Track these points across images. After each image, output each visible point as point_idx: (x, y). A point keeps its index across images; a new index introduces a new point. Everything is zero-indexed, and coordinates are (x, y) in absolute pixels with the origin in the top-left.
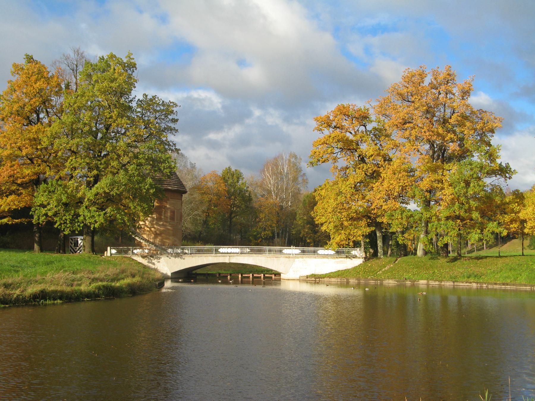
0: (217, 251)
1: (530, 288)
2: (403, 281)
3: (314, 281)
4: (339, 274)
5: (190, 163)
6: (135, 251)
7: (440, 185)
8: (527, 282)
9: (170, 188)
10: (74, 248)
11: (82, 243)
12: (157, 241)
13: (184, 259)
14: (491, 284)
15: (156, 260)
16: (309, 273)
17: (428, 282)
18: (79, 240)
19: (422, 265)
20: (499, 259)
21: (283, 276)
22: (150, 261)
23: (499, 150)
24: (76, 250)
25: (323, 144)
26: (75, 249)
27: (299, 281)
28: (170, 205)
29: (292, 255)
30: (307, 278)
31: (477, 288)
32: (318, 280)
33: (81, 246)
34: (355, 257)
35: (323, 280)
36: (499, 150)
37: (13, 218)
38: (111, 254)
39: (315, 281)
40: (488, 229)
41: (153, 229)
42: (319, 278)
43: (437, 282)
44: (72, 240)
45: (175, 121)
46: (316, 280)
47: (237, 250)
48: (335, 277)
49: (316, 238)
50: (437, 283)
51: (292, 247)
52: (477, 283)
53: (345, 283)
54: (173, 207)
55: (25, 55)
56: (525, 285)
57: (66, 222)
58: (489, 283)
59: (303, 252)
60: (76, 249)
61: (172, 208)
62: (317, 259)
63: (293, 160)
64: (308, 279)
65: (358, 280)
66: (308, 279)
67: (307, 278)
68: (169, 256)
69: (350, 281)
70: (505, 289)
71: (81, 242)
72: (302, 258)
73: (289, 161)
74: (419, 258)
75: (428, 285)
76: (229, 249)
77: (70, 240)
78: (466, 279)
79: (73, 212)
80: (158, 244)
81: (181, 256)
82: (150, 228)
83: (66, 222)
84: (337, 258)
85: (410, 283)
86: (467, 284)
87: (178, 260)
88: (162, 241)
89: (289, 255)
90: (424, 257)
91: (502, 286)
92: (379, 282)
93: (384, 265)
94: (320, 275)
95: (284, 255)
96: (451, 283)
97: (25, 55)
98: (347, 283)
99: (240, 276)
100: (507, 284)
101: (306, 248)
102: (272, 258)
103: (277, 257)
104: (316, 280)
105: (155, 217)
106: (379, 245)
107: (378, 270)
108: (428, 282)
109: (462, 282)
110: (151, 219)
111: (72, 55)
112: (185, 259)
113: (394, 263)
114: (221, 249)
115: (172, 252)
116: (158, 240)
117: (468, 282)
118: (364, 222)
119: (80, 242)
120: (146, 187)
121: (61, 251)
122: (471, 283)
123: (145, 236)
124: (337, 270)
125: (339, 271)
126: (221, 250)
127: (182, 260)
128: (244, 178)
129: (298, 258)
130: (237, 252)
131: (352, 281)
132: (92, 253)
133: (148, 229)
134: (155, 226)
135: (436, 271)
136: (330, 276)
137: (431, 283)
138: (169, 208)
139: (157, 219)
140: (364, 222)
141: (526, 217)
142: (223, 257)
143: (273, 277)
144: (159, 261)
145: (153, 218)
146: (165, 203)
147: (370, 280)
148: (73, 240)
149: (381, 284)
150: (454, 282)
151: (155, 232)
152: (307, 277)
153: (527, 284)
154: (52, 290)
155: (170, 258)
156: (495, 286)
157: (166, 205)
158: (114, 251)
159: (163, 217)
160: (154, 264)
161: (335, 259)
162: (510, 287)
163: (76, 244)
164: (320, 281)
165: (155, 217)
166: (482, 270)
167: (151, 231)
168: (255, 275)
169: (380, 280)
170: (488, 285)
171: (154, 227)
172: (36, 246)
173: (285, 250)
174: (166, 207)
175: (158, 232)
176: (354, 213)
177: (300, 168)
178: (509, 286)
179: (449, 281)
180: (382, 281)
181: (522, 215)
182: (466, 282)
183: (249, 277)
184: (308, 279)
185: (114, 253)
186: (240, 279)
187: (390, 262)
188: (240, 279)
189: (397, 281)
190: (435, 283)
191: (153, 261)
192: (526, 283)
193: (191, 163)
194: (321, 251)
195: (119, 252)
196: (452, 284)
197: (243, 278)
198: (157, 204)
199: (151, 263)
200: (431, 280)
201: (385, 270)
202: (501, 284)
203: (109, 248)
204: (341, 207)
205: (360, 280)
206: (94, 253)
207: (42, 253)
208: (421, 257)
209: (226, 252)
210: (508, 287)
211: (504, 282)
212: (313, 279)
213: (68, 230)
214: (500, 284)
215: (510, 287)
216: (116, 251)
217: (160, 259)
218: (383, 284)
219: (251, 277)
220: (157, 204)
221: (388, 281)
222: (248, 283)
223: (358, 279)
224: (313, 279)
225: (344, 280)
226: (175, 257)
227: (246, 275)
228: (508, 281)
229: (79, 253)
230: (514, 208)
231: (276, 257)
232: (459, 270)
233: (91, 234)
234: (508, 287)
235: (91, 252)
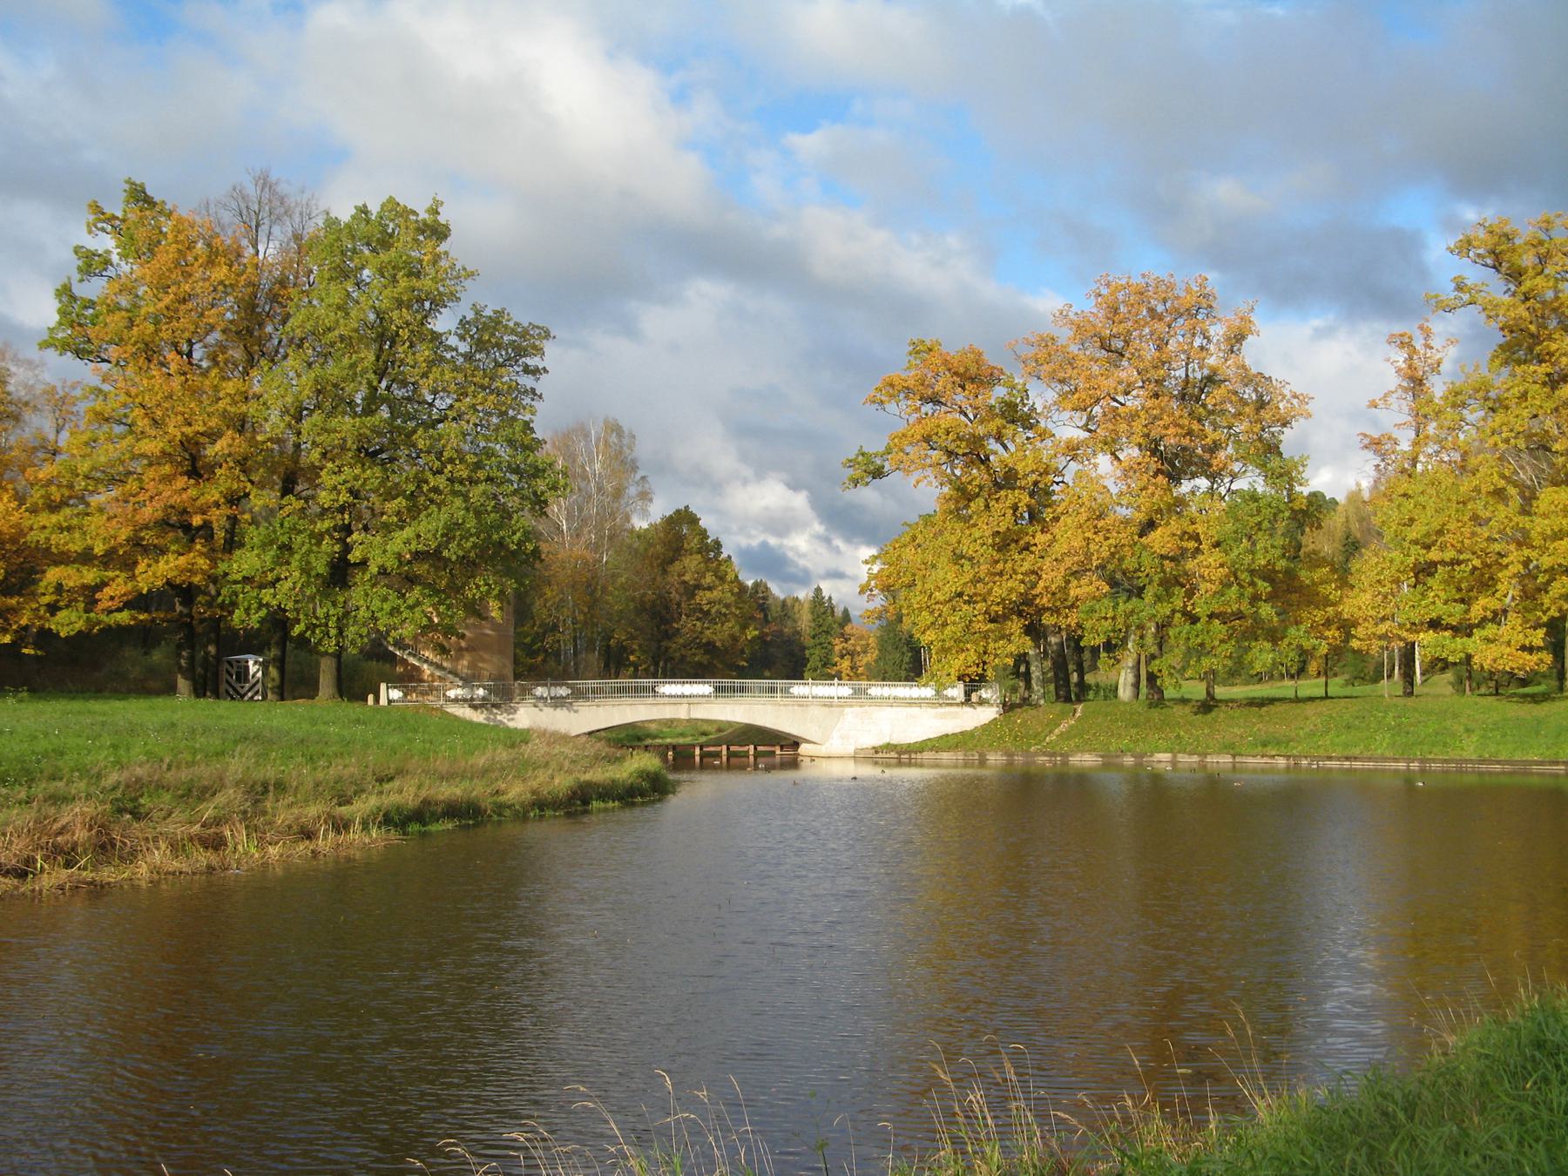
2: (1117, 757)
7: (1192, 545)
10: (237, 686)
11: (260, 672)
13: (576, 711)
14: (1320, 758)
15: (505, 715)
17: (1175, 756)
18: (251, 663)
20: (1328, 701)
22: (492, 717)
23: (1303, 466)
24: (242, 691)
26: (239, 689)
27: (855, 762)
30: (877, 752)
32: (907, 756)
33: (258, 681)
35: (919, 756)
36: (1303, 466)
38: (390, 701)
39: (899, 758)
42: (909, 752)
44: (232, 666)
45: (534, 372)
47: (703, 688)
49: (675, 651)
50: (1195, 758)
52: (1288, 757)
55: (126, 182)
56: (1396, 760)
59: (719, 690)
60: (242, 687)
62: (894, 709)
63: (613, 439)
65: (1009, 756)
66: (880, 755)
67: (877, 752)
68: (540, 704)
71: (258, 670)
72: (861, 706)
73: (606, 443)
75: (1174, 763)
77: (226, 666)
78: (1260, 748)
81: (571, 703)
84: (941, 705)
86: (1265, 760)
88: (472, 665)
97: (126, 182)
100: (1356, 759)
101: (727, 682)
102: (791, 708)
103: (803, 706)
106: (1033, 676)
108: (1175, 756)
111: (251, 191)
112: (580, 712)
116: (465, 663)
117: (1266, 756)
119: (253, 668)
125: (947, 735)
129: (852, 706)
135: (1182, 733)
141: (1358, 614)
142: (672, 706)
143: (778, 752)
144: (511, 716)
147: (1036, 754)
148: (235, 664)
149: (1065, 763)
150: (1234, 756)
152: (876, 750)
154: (613, 781)
155: (541, 710)
158: (396, 694)
161: (936, 708)
163: (243, 674)
169: (1061, 755)
172: (183, 684)
176: (998, 604)
177: (634, 461)
180: (1065, 756)
181: (1347, 610)
182: (1263, 756)
183: (746, 755)
184: (877, 756)
185: (396, 698)
186: (697, 759)
188: (697, 759)
189: (1101, 756)
197: (730, 755)
200: (1179, 752)
203: (383, 686)
209: (701, 693)
210: (1357, 765)
211: (1346, 754)
214: (1338, 759)
217: (515, 711)
219: (724, 752)
222: (743, 768)
225: (973, 755)
226: (556, 707)
228: (1356, 751)
229: (252, 698)
230: (1331, 593)
231: (800, 706)
234: (1357, 765)
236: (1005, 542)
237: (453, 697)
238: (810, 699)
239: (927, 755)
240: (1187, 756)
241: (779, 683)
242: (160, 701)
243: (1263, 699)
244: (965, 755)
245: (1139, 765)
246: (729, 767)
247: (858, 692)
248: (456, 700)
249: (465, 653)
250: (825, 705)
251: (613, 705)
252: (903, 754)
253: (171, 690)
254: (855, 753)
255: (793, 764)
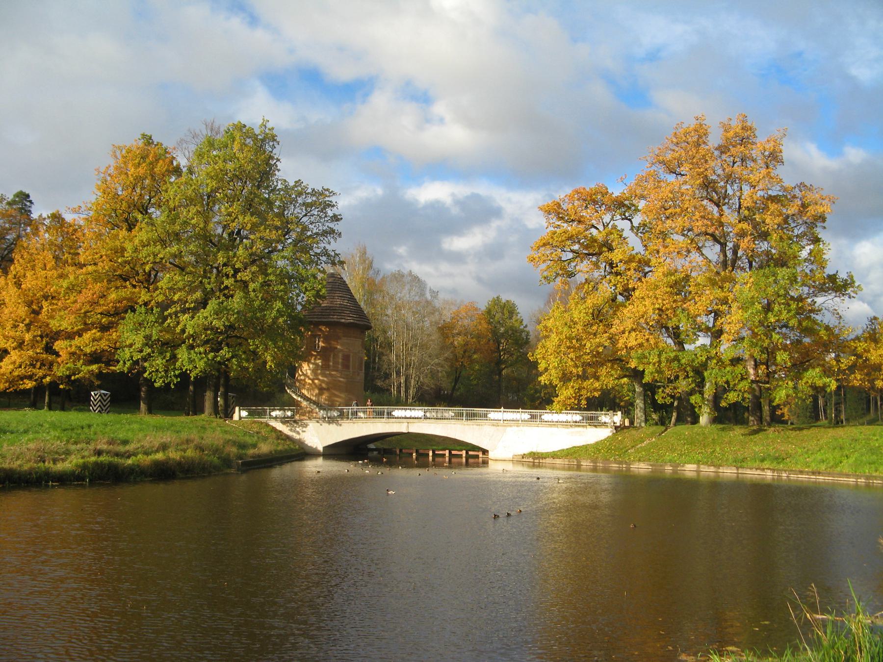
0: (390, 415)
1: (854, 480)
2: (661, 466)
3: (532, 463)
4: (572, 453)
5: (430, 290)
6: (274, 414)
8: (851, 470)
9: (343, 320)
12: (323, 399)
13: (341, 425)
14: (795, 472)
16: (526, 451)
17: (699, 467)
19: (701, 439)
21: (491, 455)
25: (544, 245)
27: (513, 463)
28: (342, 345)
29: (502, 422)
30: (523, 458)
31: (773, 479)
32: (537, 461)
34: (605, 424)
35: (544, 461)
37: (878, 411)
38: (240, 418)
39: (534, 462)
40: (805, 380)
41: (316, 381)
42: (539, 458)
43: (712, 467)
46: (535, 461)
47: (418, 412)
48: (562, 457)
50: (712, 469)
51: (502, 409)
52: (773, 470)
53: (575, 466)
54: (347, 348)
56: (848, 476)
57: (36, 364)
58: (792, 471)
61: (346, 350)
64: (524, 460)
66: (524, 460)
67: (523, 458)
68: (320, 421)
69: (582, 463)
70: (816, 482)
72: (517, 426)
74: (702, 427)
76: (408, 411)
79: (168, 355)
80: (324, 403)
82: (313, 380)
83: (36, 364)
85: (671, 468)
86: (759, 472)
87: (333, 427)
89: (497, 422)
90: (709, 426)
91: (812, 477)
92: (624, 466)
93: (642, 438)
94: (542, 454)
95: (490, 421)
96: (733, 470)
98: (577, 467)
99: (431, 453)
100: (819, 473)
102: (472, 426)
103: (479, 425)
104: (535, 461)
105: (320, 364)
107: (630, 447)
108: (699, 467)
109: (751, 469)
110: (314, 366)
113: (660, 435)
114: (396, 411)
115: (325, 416)
118: (606, 369)
120: (272, 315)
121: (191, 413)
122: (763, 470)
123: (305, 392)
124: (571, 447)
126: (396, 413)
127: (339, 427)
128: (519, 313)
129: (511, 426)
130: (420, 417)
131: (586, 463)
132: (214, 416)
133: (310, 382)
134: (320, 377)
136: (554, 455)
137: (704, 468)
138: (341, 351)
139: (322, 366)
140: (606, 369)
142: (398, 424)
143: (481, 456)
144: (304, 429)
145: (317, 365)
146: (335, 343)
147: (611, 462)
149: (628, 469)
150: (738, 468)
151: (321, 385)
152: (523, 456)
153: (850, 473)
155: (321, 425)
156: (800, 476)
157: (336, 346)
158: (244, 413)
159: (331, 364)
160: (298, 433)
162: (823, 478)
164: (539, 463)
165: (320, 364)
166: (790, 448)
167: (315, 384)
168: (453, 452)
169: (626, 463)
170: (790, 474)
171: (318, 379)
173: (492, 413)
174: (337, 348)
175: (324, 385)
178: (822, 476)
179: (731, 466)
180: (628, 464)
182: (757, 469)
185: (244, 416)
187: (653, 434)
189: (651, 465)
190: (709, 469)
191: (298, 429)
192: (849, 471)
193: (431, 290)
194: (547, 417)
195: (251, 414)
196: (736, 472)
198: (323, 345)
199: (295, 431)
200: (703, 464)
201: (641, 447)
202: (810, 472)
203: (237, 409)
204: (575, 343)
205: (596, 463)
206: (217, 416)
207: (52, 412)
208: (706, 427)
209: (403, 416)
212: (531, 460)
213: (161, 382)
214: (807, 473)
215: (823, 478)
216: (247, 414)
218: (677, 473)
219: (447, 455)
220: (323, 345)
221: (638, 465)
222: (460, 465)
223: (595, 461)
224: (531, 460)
226: (329, 423)
227: (441, 452)
228: (823, 467)
231: (477, 425)
232: (754, 448)
233: (213, 388)
234: (821, 478)
235: (213, 414)
236: (598, 315)
237: (274, 416)
238: (520, 422)
239: (548, 461)
240: (706, 467)
241: (386, 408)
242: (181, 419)
243: (35, 405)
244: (569, 462)
245: (675, 472)
246: (467, 464)
247: (533, 417)
248: (276, 418)
249: (325, 392)
250: (494, 425)
251: (363, 423)
252: (535, 459)
253: (198, 409)
254: (513, 458)
255: (485, 463)
